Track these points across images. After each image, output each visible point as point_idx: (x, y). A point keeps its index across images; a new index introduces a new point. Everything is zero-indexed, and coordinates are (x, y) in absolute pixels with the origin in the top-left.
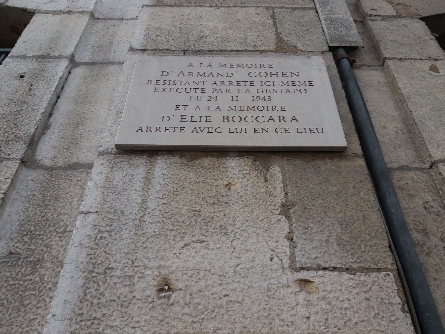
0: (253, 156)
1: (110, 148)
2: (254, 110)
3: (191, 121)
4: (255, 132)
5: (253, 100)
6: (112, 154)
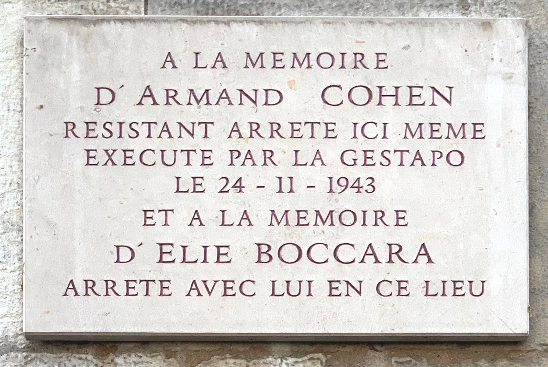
0: (325, 354)
1: (11, 334)
2: (332, 224)
3: (184, 261)
4: (331, 295)
5: (331, 191)
6: (18, 350)
